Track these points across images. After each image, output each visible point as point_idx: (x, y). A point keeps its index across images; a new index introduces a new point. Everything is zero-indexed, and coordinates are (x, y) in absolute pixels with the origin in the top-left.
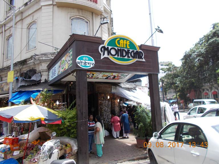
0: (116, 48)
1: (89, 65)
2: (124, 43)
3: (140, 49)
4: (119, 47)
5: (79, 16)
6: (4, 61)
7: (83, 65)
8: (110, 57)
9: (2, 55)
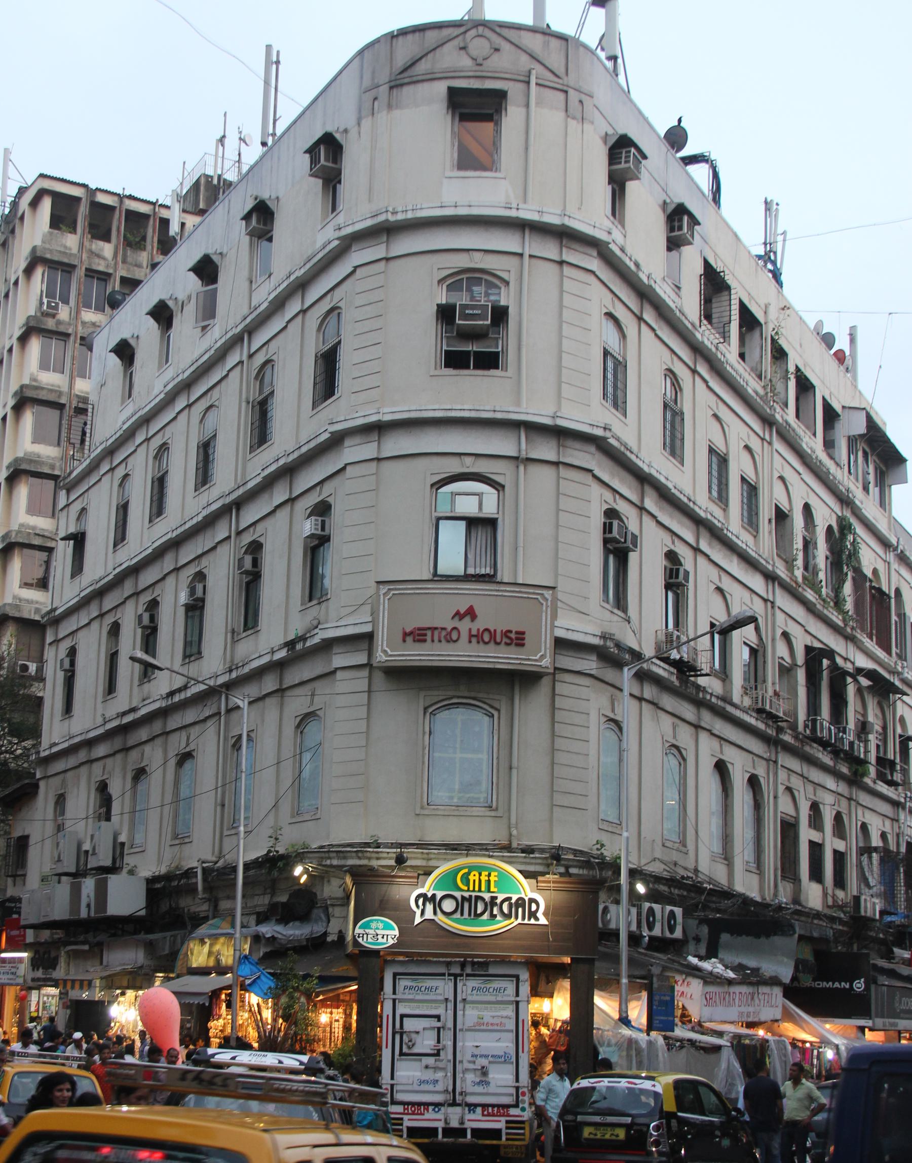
0: (458, 894)
1: (384, 940)
2: (480, 881)
3: (532, 891)
4: (463, 890)
5: (459, 697)
6: (226, 833)
7: (370, 940)
8: (441, 918)
9: (219, 808)
